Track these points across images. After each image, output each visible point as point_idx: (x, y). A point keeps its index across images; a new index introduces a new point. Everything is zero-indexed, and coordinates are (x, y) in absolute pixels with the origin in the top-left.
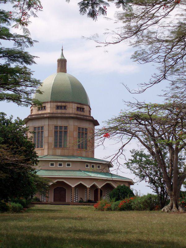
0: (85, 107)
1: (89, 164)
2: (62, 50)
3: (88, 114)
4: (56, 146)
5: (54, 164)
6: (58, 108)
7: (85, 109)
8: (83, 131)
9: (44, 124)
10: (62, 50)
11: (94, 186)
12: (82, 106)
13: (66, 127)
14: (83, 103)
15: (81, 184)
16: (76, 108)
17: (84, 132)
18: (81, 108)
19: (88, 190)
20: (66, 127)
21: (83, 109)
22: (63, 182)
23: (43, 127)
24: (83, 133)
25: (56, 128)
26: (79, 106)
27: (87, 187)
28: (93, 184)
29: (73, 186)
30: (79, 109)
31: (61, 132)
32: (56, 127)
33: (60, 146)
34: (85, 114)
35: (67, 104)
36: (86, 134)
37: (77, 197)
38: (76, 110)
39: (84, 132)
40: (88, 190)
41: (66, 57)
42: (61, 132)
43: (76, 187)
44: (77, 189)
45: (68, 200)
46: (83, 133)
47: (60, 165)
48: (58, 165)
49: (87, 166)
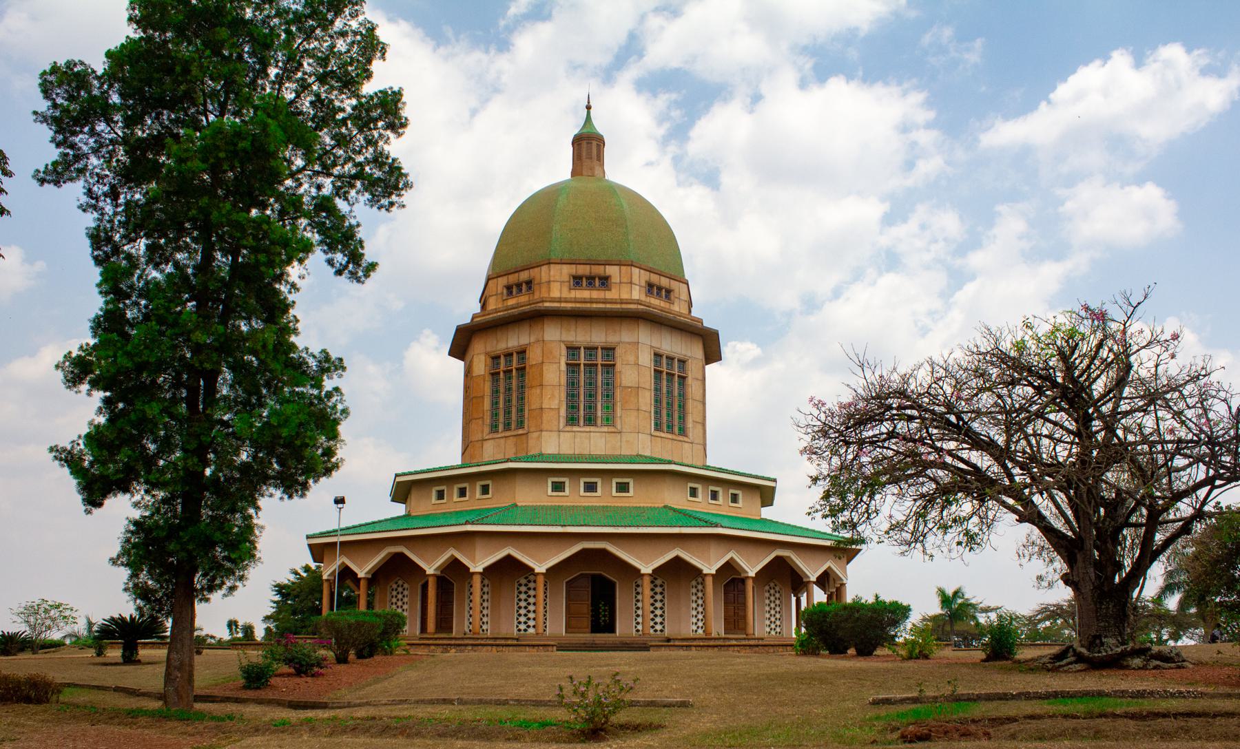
0: (674, 285)
1: (699, 486)
2: (589, 108)
3: (685, 311)
4: (658, 427)
6: (578, 283)
8: (672, 368)
9: (527, 342)
10: (589, 108)
11: (729, 567)
12: (599, 270)
13: (609, 350)
14: (603, 258)
15: (677, 558)
16: (643, 284)
17: (676, 372)
18: (519, 285)
20: (609, 350)
23: (524, 352)
24: (498, 373)
26: (583, 270)
27: (537, 570)
28: (727, 563)
29: (540, 568)
30: (514, 290)
31: (591, 367)
32: (572, 349)
34: (676, 308)
35: (534, 273)
36: (610, 368)
38: (565, 289)
39: (676, 372)
40: (709, 581)
41: (600, 126)
43: (488, 571)
45: (625, 627)
46: (661, 372)
48: (582, 489)
49: (694, 492)
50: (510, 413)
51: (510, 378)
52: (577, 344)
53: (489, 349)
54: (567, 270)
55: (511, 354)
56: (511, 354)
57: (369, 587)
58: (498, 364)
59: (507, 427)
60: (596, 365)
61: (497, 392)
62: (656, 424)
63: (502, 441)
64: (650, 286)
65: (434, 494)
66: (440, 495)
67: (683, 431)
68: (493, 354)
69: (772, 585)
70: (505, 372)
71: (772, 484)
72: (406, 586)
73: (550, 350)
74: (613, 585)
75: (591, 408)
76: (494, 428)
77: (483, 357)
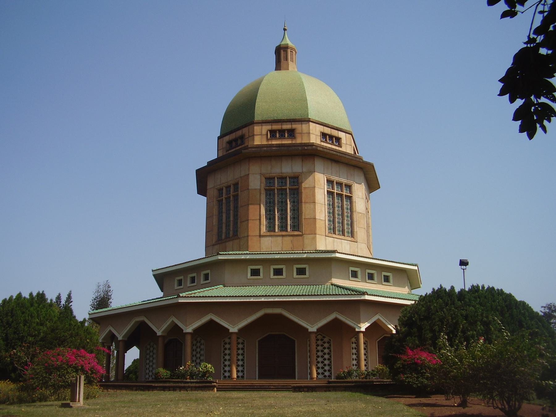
0: (341, 135)
2: (285, 30)
5: (261, 271)
7: (343, 141)
11: (375, 327)
12: (335, 133)
19: (313, 338)
21: (338, 140)
22: (281, 316)
25: (294, 182)
26: (327, 131)
29: (313, 329)
32: (270, 179)
33: (283, 227)
37: (327, 362)
42: (282, 192)
43: (197, 331)
44: (326, 340)
47: (278, 272)
50: (229, 225)
51: (222, 205)
52: (284, 175)
53: (264, 171)
54: (266, 128)
55: (230, 186)
56: (230, 186)
57: (192, 338)
58: (230, 191)
59: (283, 227)
60: (286, 189)
61: (222, 212)
62: (330, 229)
63: (280, 239)
64: (324, 135)
65: (176, 283)
66: (193, 280)
67: (352, 234)
68: (268, 176)
69: (199, 339)
70: (234, 196)
71: (416, 268)
72: (202, 341)
73: (255, 178)
74: (294, 342)
75: (283, 219)
76: (271, 227)
77: (258, 177)
